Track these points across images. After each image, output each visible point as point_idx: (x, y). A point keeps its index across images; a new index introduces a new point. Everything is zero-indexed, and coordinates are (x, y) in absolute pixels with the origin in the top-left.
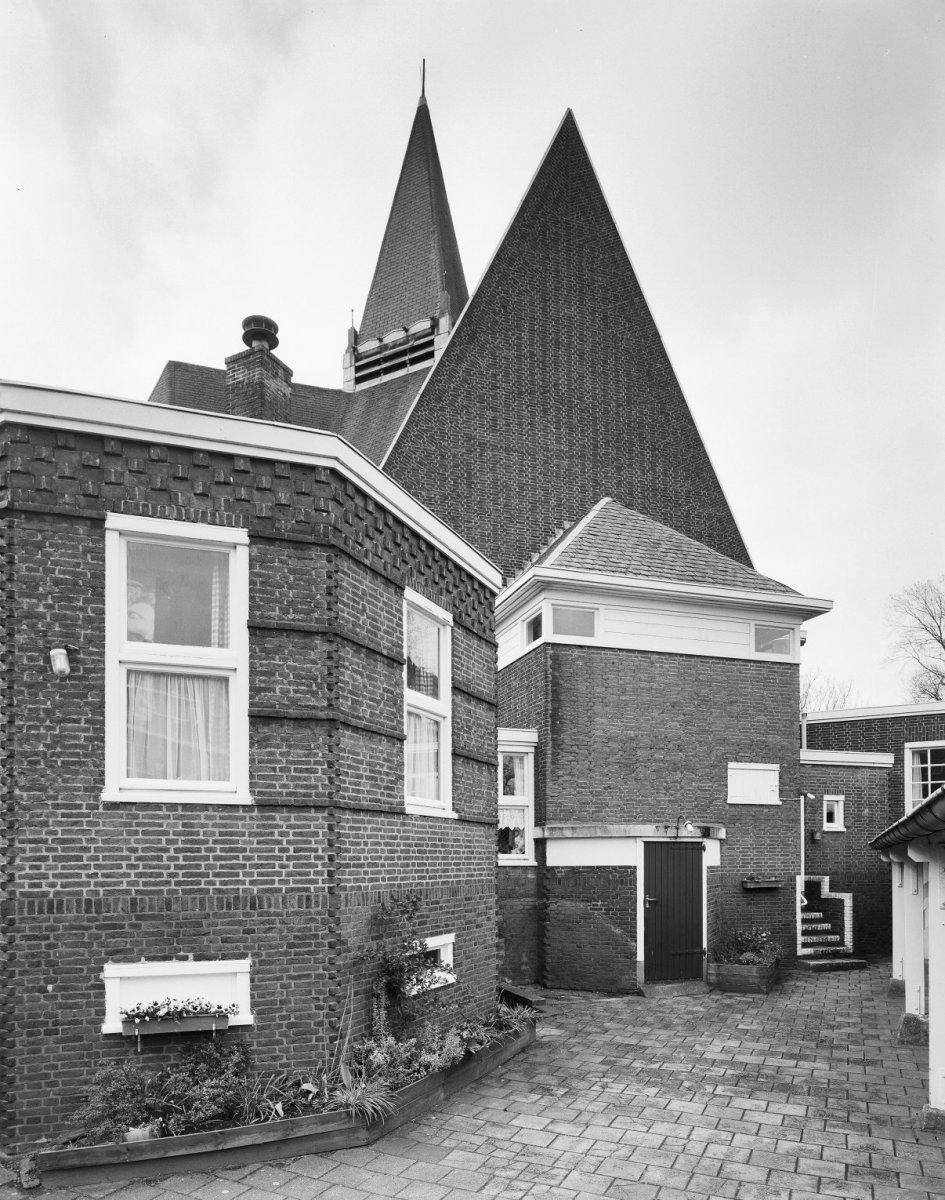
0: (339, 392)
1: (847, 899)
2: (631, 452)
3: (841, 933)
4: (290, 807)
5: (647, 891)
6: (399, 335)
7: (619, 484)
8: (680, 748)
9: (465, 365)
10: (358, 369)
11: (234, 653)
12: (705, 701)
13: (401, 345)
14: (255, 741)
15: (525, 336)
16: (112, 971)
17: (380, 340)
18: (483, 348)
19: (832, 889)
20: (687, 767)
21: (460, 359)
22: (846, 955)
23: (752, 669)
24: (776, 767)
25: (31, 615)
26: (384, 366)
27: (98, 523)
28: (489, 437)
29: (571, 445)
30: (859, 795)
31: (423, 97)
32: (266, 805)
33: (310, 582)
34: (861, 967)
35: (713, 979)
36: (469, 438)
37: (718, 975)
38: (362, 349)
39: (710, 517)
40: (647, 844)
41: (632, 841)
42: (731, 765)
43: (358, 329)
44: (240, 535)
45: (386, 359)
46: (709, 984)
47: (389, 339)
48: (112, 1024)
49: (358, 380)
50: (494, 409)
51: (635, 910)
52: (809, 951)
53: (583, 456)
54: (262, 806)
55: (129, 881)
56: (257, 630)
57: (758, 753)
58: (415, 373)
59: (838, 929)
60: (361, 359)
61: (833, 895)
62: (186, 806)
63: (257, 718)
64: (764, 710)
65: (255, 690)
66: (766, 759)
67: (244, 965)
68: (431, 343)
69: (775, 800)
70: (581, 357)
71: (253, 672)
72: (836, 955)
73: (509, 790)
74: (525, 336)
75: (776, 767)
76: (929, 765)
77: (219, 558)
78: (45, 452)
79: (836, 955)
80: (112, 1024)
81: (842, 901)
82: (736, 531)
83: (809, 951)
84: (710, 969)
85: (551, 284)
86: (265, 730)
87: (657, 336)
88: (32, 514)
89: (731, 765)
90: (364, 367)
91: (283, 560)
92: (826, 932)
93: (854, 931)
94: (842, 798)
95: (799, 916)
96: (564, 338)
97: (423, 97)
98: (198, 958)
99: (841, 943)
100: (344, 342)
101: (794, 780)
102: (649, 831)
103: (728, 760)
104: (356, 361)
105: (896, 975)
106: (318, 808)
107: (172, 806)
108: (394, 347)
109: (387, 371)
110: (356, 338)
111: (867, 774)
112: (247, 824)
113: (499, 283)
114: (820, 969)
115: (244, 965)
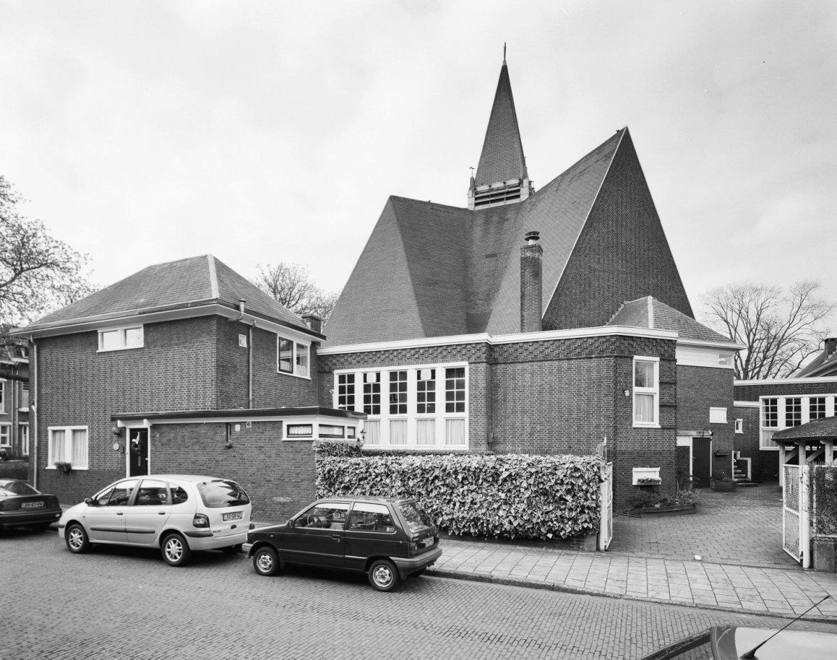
0: (466, 210)
1: (749, 460)
2: (649, 270)
3: (746, 473)
4: (667, 428)
5: (693, 455)
6: (500, 185)
7: (644, 284)
8: (694, 402)
9: (588, 237)
10: (476, 199)
11: (656, 389)
12: (702, 384)
13: (501, 189)
14: (661, 412)
15: (610, 223)
16: (634, 469)
17: (490, 186)
18: (595, 229)
19: (741, 456)
20: (697, 409)
21: (587, 235)
22: (749, 482)
23: (718, 372)
24: (726, 409)
25: (620, 382)
26: (492, 199)
27: (632, 358)
28: (597, 267)
29: (627, 268)
30: (748, 419)
31: (505, 61)
32: (663, 428)
33: (672, 370)
34: (756, 486)
35: (713, 487)
36: (590, 267)
37: (716, 486)
38: (480, 189)
39: (678, 298)
40: (693, 438)
41: (688, 437)
42: (711, 408)
43: (474, 177)
44: (658, 359)
45: (492, 196)
46: (713, 489)
47: (495, 186)
48: (635, 483)
49: (476, 204)
50: (599, 255)
51: (689, 462)
52: (736, 480)
53: (631, 273)
54: (663, 428)
55: (637, 447)
56: (661, 383)
57: (719, 403)
58: (510, 205)
59: (746, 472)
60: (478, 194)
61: (742, 459)
62: (648, 429)
63: (661, 406)
64: (722, 387)
65: (660, 399)
66: (722, 406)
67: (658, 469)
68: (519, 191)
69: (725, 422)
70: (631, 230)
71: (660, 394)
72: (745, 481)
73: (737, 429)
74: (610, 223)
75: (726, 409)
76: (770, 406)
77: (651, 364)
78: (622, 341)
79: (745, 481)
80: (635, 483)
81: (746, 461)
82: (688, 303)
83: (736, 480)
84: (713, 484)
85: (620, 201)
86: (663, 409)
87: (659, 220)
88: (621, 357)
89: (711, 408)
90: (479, 199)
91: (666, 363)
92: (741, 473)
93: (752, 472)
94: (741, 420)
95: (733, 467)
96: (624, 223)
97: (505, 61)
98: (650, 467)
99: (747, 477)
100: (468, 185)
101: (732, 414)
102: (694, 433)
103: (710, 406)
104: (476, 194)
105: (780, 485)
106: (672, 429)
107: (645, 428)
108: (497, 190)
109: (492, 201)
110: (474, 184)
111: (751, 410)
112: (659, 433)
113: (601, 202)
114: (742, 486)
115: (658, 469)
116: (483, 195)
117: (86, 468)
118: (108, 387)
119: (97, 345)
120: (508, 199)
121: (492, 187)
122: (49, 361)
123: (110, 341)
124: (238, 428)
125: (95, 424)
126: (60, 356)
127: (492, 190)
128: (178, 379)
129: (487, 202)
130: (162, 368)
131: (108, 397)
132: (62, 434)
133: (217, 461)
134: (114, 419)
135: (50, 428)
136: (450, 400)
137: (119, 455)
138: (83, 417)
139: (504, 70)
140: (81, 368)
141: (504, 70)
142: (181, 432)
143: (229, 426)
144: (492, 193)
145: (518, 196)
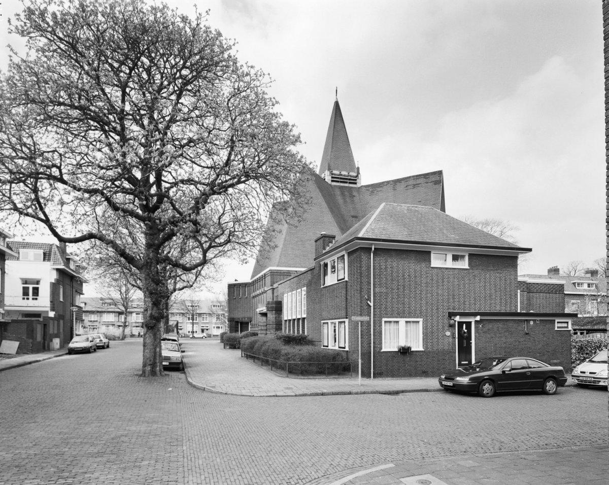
6: (346, 174)
10: (332, 177)
45: (341, 178)
49: (332, 181)
108: (344, 176)
109: (341, 182)
116: (335, 176)
117: (421, 349)
118: (440, 292)
119: (430, 261)
120: (350, 183)
121: (342, 173)
122: (383, 267)
123: (436, 261)
124: (532, 323)
125: (429, 318)
126: (395, 264)
127: (341, 175)
128: (493, 292)
129: (338, 182)
130: (482, 284)
131: (440, 298)
132: (417, 324)
133: (519, 342)
134: (451, 315)
135: (384, 320)
136: (35, 296)
137: (451, 340)
138: (418, 312)
139: (337, 106)
140: (415, 277)
141: (337, 106)
142: (496, 325)
143: (528, 321)
144: (341, 177)
145: (356, 183)
